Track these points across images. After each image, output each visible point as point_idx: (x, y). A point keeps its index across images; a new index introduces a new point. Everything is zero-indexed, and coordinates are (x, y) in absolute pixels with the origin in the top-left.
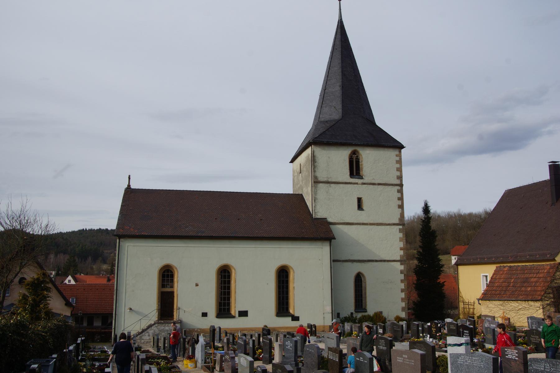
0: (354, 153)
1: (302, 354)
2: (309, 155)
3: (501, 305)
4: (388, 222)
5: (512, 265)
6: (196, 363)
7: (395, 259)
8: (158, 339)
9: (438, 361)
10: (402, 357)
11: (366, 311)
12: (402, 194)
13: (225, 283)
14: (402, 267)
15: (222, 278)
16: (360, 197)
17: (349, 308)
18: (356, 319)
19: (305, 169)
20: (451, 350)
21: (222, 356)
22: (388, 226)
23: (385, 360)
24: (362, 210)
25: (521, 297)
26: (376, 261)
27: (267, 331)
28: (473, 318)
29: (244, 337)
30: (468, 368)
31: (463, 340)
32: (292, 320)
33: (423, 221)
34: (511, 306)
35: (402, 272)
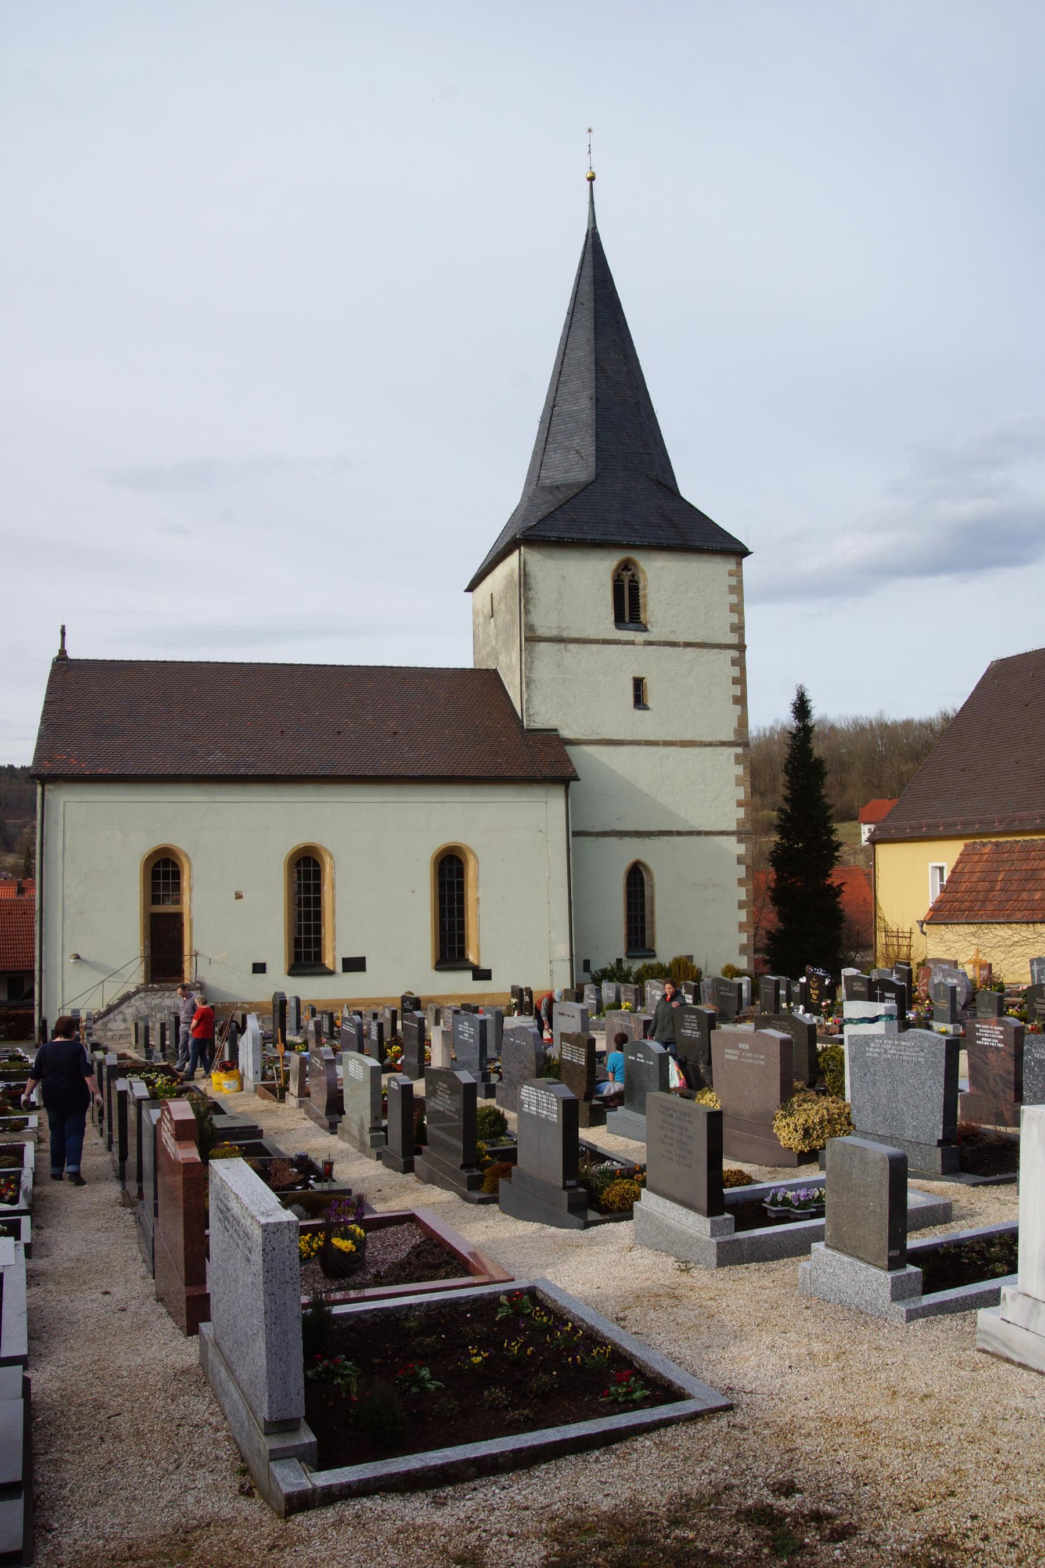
0: (626, 566)
1: (499, 1054)
2: (513, 570)
3: (973, 934)
4: (709, 739)
5: (1001, 840)
6: (241, 1079)
7: (723, 828)
8: (147, 1028)
9: (821, 1060)
10: (736, 1048)
11: (654, 956)
12: (743, 670)
13: (307, 891)
14: (741, 849)
15: (299, 879)
16: (639, 675)
17: (612, 946)
18: (629, 973)
19: (503, 607)
20: (849, 1030)
21: (303, 1062)
22: (708, 749)
23: (697, 1062)
24: (646, 708)
25: (1018, 915)
26: (679, 833)
27: (412, 1003)
28: (908, 964)
29: (357, 1018)
30: (889, 1067)
31: (879, 1008)
32: (475, 978)
33: (794, 737)
34: (996, 936)
35: (740, 860)
